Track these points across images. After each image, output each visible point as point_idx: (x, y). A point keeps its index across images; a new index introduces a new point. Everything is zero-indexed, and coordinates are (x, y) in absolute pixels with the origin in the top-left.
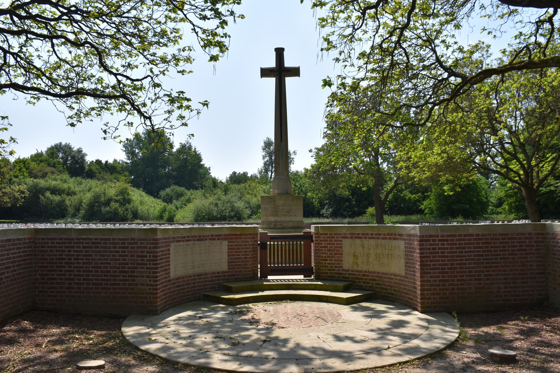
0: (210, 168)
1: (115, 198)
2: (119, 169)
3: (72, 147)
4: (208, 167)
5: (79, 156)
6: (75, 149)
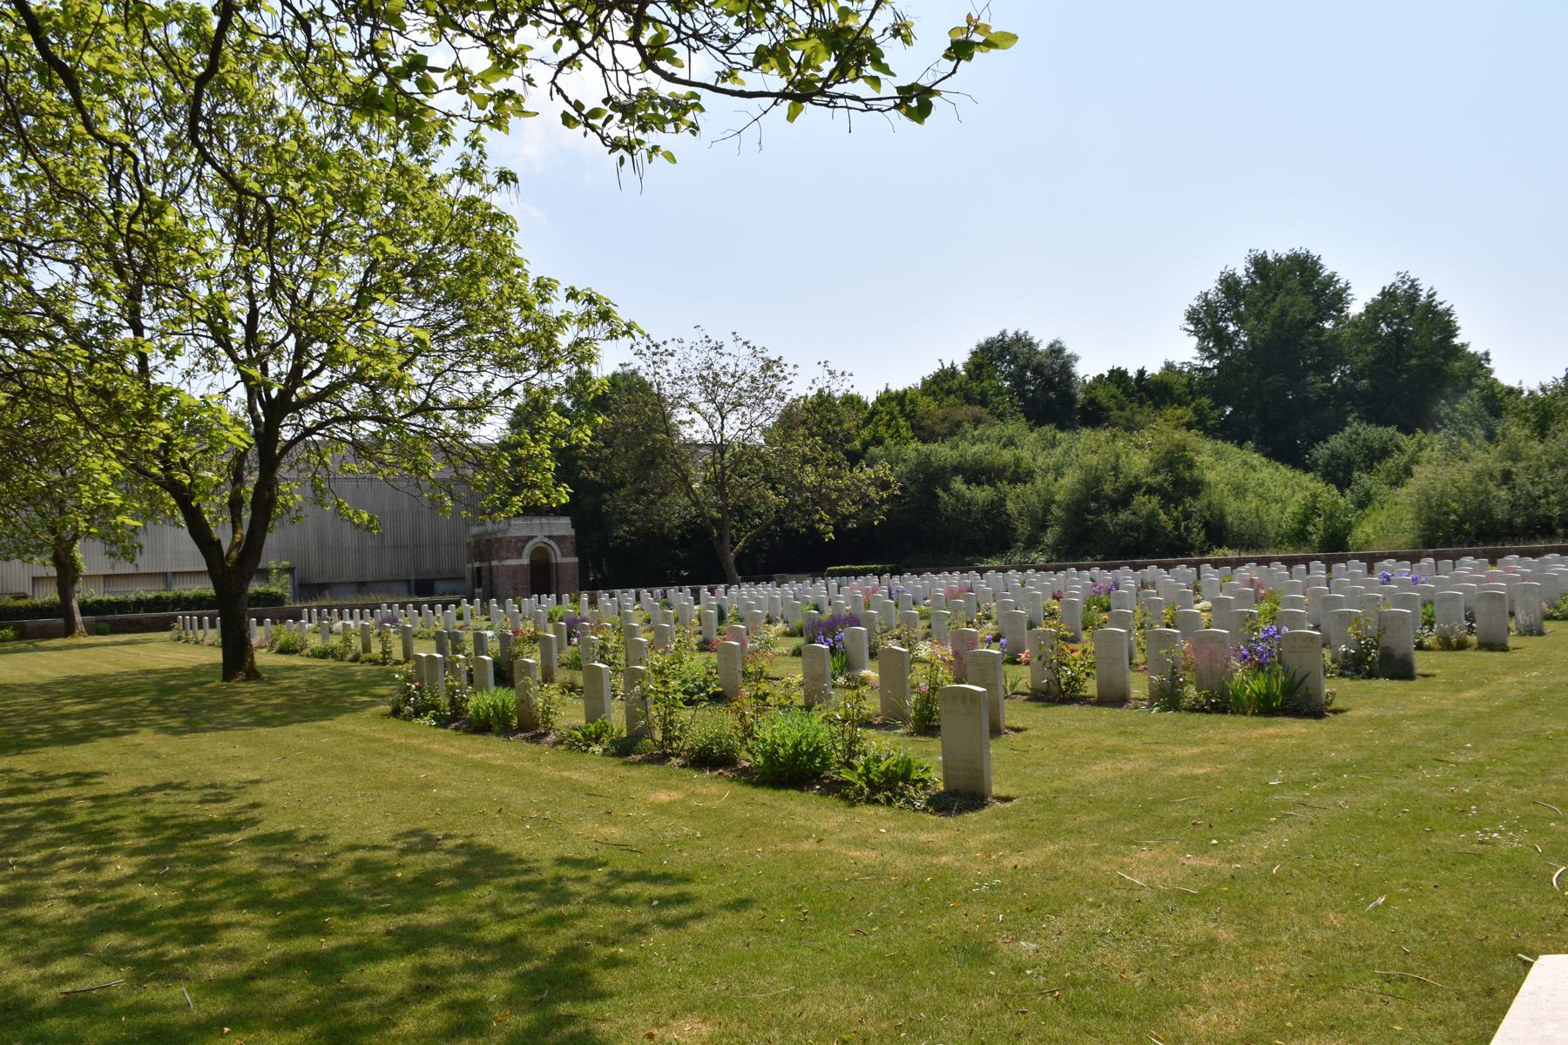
0: (1487, 354)
1: (1149, 479)
2: (1179, 390)
3: (1035, 341)
4: (1481, 351)
5: (1058, 363)
6: (1043, 347)
